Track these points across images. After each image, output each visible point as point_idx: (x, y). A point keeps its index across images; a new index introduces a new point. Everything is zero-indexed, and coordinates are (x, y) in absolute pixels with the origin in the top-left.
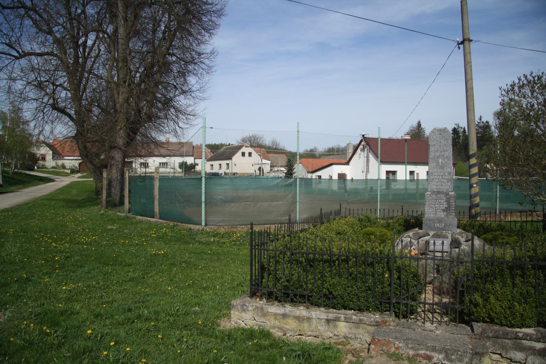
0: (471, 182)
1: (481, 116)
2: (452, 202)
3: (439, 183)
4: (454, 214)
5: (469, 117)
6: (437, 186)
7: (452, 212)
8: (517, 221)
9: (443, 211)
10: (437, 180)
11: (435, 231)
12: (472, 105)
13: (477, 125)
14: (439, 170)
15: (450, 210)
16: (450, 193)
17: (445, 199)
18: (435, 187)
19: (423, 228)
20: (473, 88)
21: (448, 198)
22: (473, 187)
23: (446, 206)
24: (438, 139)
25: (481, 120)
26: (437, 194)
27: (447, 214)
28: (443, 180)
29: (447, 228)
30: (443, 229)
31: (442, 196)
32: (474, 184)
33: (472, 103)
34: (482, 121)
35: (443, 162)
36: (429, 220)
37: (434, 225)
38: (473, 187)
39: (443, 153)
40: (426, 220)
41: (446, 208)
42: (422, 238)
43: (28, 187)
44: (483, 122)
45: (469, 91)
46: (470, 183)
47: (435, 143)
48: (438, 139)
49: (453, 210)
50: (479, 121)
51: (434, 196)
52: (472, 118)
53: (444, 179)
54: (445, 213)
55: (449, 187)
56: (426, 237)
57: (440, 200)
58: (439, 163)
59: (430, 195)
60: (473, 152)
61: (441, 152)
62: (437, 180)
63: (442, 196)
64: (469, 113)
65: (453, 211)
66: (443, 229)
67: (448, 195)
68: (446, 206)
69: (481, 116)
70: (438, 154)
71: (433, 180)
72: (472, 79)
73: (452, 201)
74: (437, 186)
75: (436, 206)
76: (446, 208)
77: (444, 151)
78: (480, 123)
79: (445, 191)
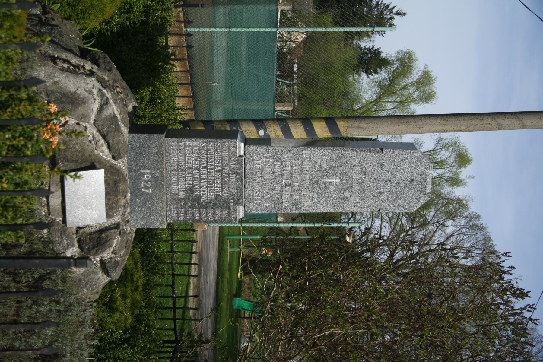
0: (271, 123)
1: (404, 14)
2: (214, 214)
3: (269, 177)
4: (181, 218)
5: (429, 121)
6: (262, 170)
7: (186, 214)
8: (174, 288)
9: (190, 191)
10: (277, 171)
11: (130, 170)
12: (458, 128)
13: (388, 6)
14: (307, 176)
15: (192, 207)
16: (241, 209)
17: (225, 194)
18: (259, 164)
19: (137, 136)
20: (499, 129)
21: (228, 203)
22: (258, 129)
23: (204, 198)
24: (398, 176)
25: (398, 14)
26: (237, 174)
27: (180, 200)
28: (278, 188)
29: (140, 201)
30: (136, 192)
31: (232, 187)
32: (265, 130)
33: (463, 127)
34: (395, 16)
35: (332, 189)
36: (160, 153)
37: (145, 168)
38: (258, 129)
39: (357, 187)
40: (161, 145)
41: (199, 197)
42: (102, 141)
43: (217, 252)
44: (391, 19)
45: (493, 123)
46: (268, 120)
47: (387, 167)
48: (398, 176)
49: (193, 215)
50: (395, 11)
51: (232, 165)
52: (426, 128)
53: (281, 191)
54: (182, 195)
55: (260, 205)
56: (107, 151)
57: (219, 181)
58: (327, 177)
59: (234, 154)
60: (342, 130)
61: (361, 183)
62: (277, 171)
63: (232, 187)
64: (438, 121)
65: (189, 216)
66: (136, 192)
67: (237, 203)
68: (204, 198)
69: (404, 14)
70: (355, 175)
71: (279, 159)
72: (524, 127)
73: (218, 212)
74: (262, 170)
75: (204, 171)
76: (199, 197)
77: (362, 191)
78: (391, 11)
79: (247, 192)
